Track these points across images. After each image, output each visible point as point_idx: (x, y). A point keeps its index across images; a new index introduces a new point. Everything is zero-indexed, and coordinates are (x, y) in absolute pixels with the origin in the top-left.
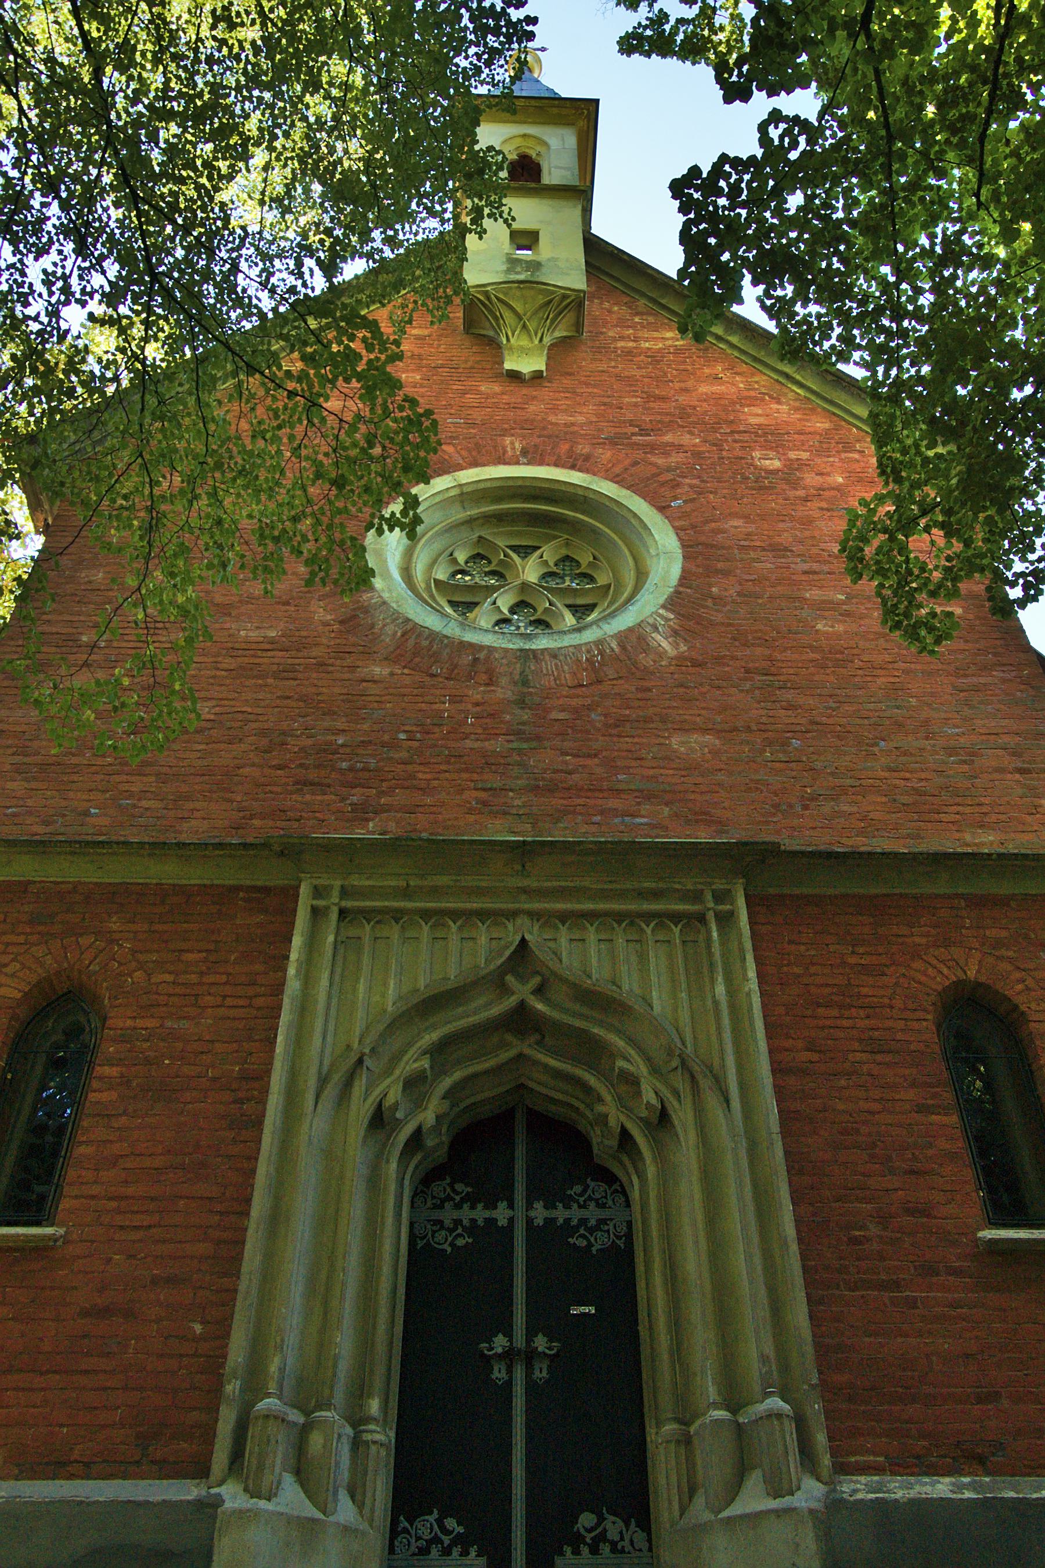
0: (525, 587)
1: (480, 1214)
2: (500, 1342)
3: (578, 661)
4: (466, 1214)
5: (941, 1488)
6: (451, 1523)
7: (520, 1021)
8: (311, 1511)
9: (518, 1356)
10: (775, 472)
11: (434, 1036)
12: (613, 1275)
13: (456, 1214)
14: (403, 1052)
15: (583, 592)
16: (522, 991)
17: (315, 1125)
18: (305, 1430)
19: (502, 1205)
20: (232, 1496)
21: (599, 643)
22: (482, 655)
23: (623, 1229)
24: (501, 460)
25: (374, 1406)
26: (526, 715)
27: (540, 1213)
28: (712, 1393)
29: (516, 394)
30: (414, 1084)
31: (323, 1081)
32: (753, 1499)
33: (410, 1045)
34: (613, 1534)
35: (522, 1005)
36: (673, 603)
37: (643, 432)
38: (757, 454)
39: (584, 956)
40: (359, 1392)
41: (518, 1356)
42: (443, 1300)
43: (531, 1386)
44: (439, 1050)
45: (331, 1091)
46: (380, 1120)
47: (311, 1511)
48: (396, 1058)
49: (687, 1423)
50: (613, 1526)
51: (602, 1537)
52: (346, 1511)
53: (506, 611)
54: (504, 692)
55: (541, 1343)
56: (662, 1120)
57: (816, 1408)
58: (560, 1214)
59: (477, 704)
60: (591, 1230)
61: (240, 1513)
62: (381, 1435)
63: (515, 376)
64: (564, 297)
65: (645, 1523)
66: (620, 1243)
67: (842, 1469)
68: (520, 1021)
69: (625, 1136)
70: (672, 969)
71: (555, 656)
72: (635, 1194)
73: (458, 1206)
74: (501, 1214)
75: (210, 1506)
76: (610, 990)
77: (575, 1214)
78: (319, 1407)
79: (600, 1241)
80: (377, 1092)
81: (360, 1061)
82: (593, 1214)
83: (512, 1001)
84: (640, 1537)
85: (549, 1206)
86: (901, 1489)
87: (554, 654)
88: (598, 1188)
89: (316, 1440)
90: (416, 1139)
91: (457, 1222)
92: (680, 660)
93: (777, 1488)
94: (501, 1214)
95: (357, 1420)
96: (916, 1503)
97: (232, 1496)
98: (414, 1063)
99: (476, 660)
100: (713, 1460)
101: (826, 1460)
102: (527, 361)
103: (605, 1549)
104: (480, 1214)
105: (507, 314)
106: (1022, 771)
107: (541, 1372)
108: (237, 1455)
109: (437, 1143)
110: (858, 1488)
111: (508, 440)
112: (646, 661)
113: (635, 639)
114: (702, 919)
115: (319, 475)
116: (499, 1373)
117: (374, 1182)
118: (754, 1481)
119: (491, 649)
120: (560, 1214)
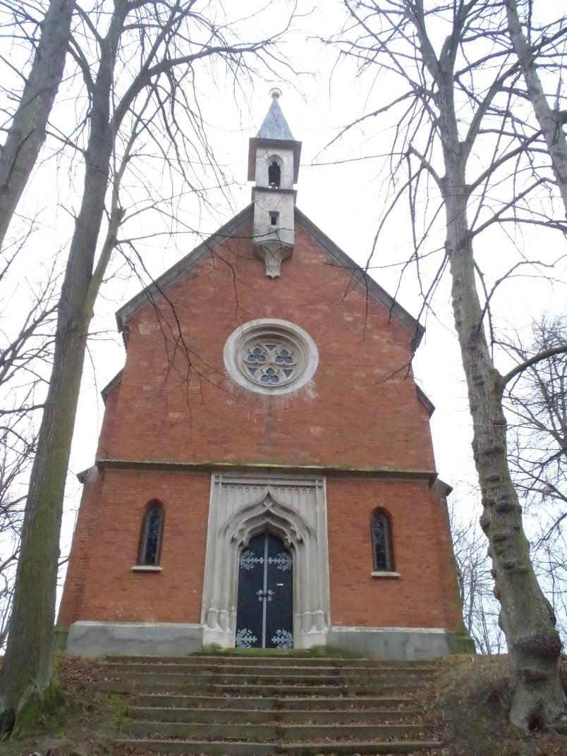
0: (271, 364)
1: (256, 560)
2: (260, 592)
3: (286, 400)
4: (253, 560)
5: (353, 629)
6: (249, 631)
7: (268, 514)
8: (222, 631)
9: (265, 594)
10: (350, 322)
11: (246, 519)
12: (288, 576)
13: (250, 560)
14: (239, 523)
15: (289, 366)
16: (268, 506)
17: (220, 542)
18: (219, 614)
19: (261, 558)
20: (205, 626)
21: (292, 393)
22: (258, 397)
23: (238, 634)
24: (265, 316)
25: (233, 608)
26: (270, 419)
27: (271, 560)
28: (308, 608)
29: (272, 283)
30: (241, 531)
31: (220, 531)
32: (314, 631)
33: (240, 521)
34: (284, 634)
35: (268, 510)
36: (315, 378)
37: (310, 303)
38: (345, 314)
39: (284, 497)
40: (230, 605)
41: (265, 594)
42: (248, 580)
43: (267, 602)
44: (248, 522)
45: (222, 533)
46: (233, 540)
47: (222, 631)
48: (237, 525)
49: (302, 613)
50: (285, 633)
51: (282, 635)
52: (228, 630)
53: (265, 372)
54: (265, 411)
55: (270, 592)
56: (301, 542)
57: (329, 613)
58: (275, 561)
59: (257, 415)
60: (246, 635)
61: (207, 631)
62: (235, 614)
63: (270, 277)
64: (286, 247)
65: (292, 632)
66: (239, 631)
67: (333, 625)
68: (268, 514)
69: (292, 544)
70: (307, 502)
71: (279, 398)
72: (294, 558)
73: (251, 558)
74: (261, 560)
75: (202, 630)
76: (290, 508)
77: (279, 561)
78: (222, 609)
79: (285, 568)
80: (233, 533)
81: (228, 526)
82: (283, 561)
83: (265, 510)
84: (290, 635)
85: (273, 558)
86: (345, 629)
87: (279, 397)
88: (284, 554)
89: (222, 616)
90: (241, 544)
91: (250, 562)
92: (316, 399)
93: (319, 628)
94: (261, 560)
95: (230, 611)
96: (348, 633)
97: (205, 626)
98: (240, 526)
99: (257, 399)
100: (307, 622)
101: (330, 623)
102: (274, 273)
103: (283, 637)
104: (256, 560)
105: (268, 252)
106: (405, 441)
107: (270, 599)
108: (206, 619)
109: (246, 544)
110: (335, 629)
111: (267, 307)
112: (305, 399)
113: (302, 392)
114: (314, 487)
115: (151, 15)
116: (260, 599)
117: (233, 556)
118: (314, 627)
119: (261, 395)
120: (275, 561)
